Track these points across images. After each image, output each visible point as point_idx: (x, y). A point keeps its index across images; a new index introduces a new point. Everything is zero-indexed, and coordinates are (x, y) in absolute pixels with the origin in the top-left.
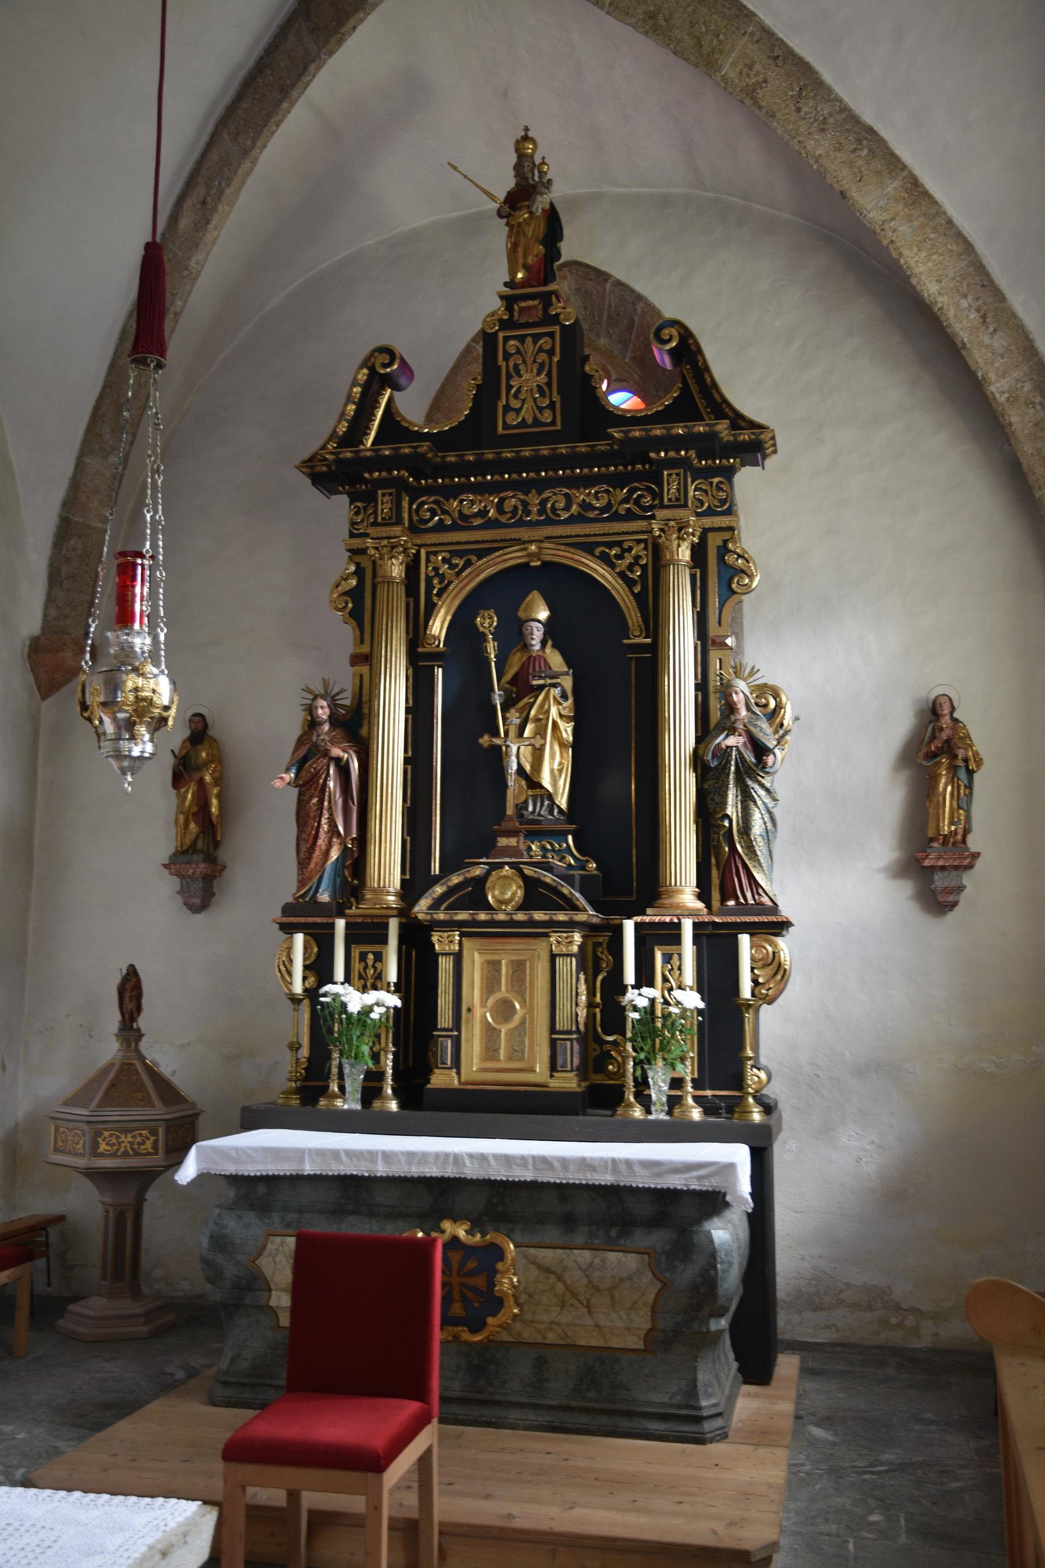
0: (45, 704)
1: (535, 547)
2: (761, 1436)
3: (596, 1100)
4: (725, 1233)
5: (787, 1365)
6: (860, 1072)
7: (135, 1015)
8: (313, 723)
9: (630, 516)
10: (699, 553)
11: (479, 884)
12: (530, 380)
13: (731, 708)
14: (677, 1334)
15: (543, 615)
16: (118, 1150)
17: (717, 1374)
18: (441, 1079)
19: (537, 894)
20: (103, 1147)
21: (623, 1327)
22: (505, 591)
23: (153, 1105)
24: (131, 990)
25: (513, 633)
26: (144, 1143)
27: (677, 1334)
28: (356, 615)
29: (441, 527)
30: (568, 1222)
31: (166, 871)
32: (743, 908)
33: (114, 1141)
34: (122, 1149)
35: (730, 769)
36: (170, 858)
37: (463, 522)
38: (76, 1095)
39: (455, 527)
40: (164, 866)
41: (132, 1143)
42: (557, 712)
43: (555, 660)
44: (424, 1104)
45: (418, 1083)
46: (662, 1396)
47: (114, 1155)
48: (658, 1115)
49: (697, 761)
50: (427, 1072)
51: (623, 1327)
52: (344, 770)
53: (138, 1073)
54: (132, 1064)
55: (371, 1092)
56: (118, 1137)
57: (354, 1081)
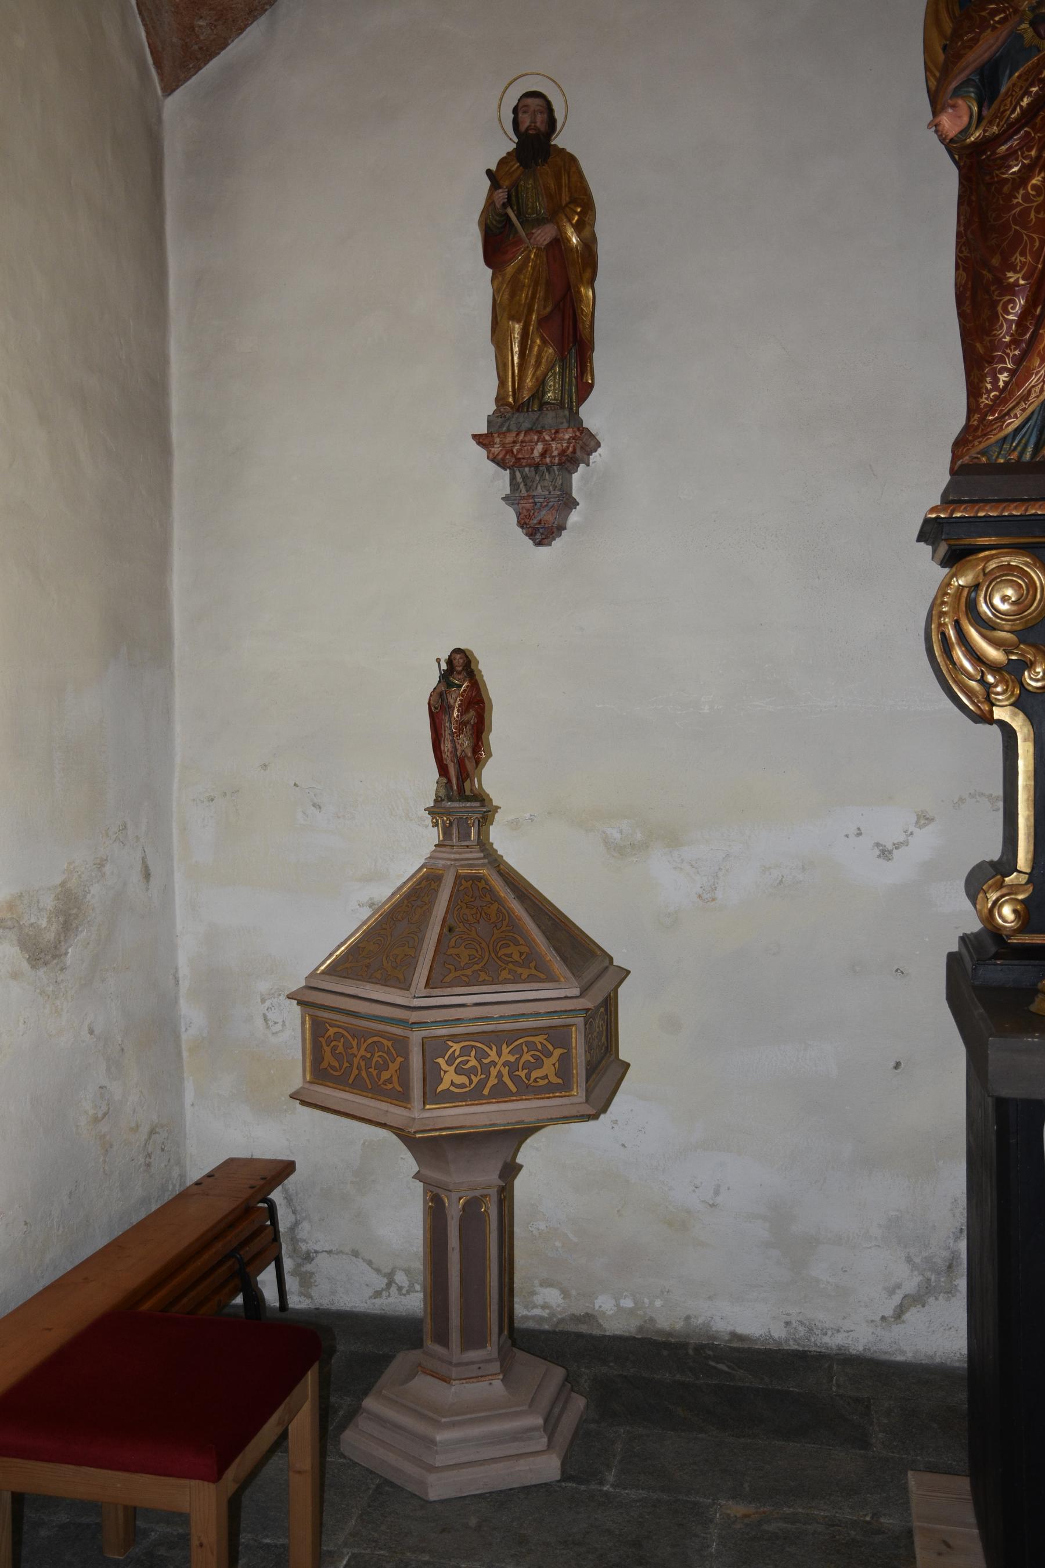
0: (173, 105)
7: (469, 765)
16: (482, 1084)
20: (450, 1077)
23: (551, 978)
26: (539, 1063)
31: (482, 452)
33: (473, 1062)
34: (493, 1081)
36: (490, 423)
38: (355, 951)
40: (478, 438)
41: (512, 1067)
47: (475, 1096)
53: (496, 899)
54: (479, 878)
56: (481, 1055)
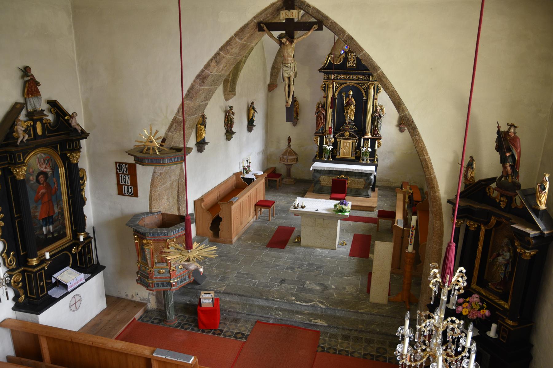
1: (353, 83)
2: (374, 197)
3: (357, 160)
4: (372, 177)
5: (376, 189)
6: (389, 152)
8: (319, 107)
9: (365, 80)
10: (374, 88)
11: (344, 134)
12: (352, 59)
13: (376, 109)
14: (366, 188)
15: (351, 93)
17: (370, 191)
18: (338, 157)
19: (351, 136)
21: (361, 186)
22: (347, 90)
24: (289, 140)
25: (347, 96)
27: (366, 188)
28: (324, 90)
29: (337, 79)
30: (355, 176)
32: (376, 136)
35: (377, 118)
37: (340, 79)
39: (339, 79)
42: (353, 108)
43: (353, 100)
44: (335, 159)
45: (334, 157)
46: (364, 193)
48: (364, 162)
49: (372, 116)
50: (336, 156)
51: (361, 186)
52: (323, 114)
55: (329, 158)
57: (327, 156)
